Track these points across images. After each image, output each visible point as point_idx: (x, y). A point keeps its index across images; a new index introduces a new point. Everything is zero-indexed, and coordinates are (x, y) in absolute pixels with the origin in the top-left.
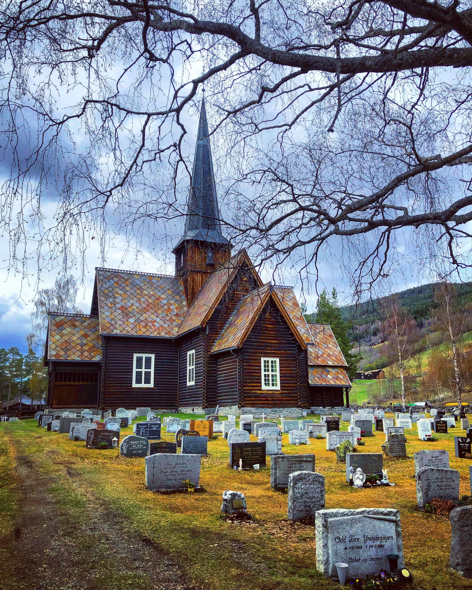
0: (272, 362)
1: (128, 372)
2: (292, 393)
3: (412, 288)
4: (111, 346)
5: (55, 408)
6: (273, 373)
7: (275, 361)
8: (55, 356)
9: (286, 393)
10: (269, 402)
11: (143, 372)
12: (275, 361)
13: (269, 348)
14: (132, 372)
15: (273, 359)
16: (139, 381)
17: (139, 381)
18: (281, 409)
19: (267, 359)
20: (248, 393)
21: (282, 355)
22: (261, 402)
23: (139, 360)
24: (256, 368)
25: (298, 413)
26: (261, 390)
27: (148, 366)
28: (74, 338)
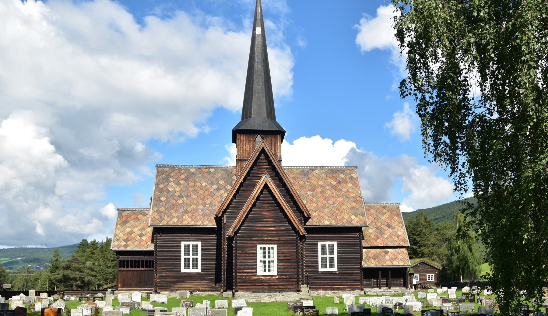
0: (269, 249)
1: (205, 256)
2: (290, 278)
3: (312, 138)
4: (161, 236)
5: (120, 290)
6: (269, 259)
7: (273, 248)
8: (124, 246)
9: (283, 278)
10: (265, 287)
11: (192, 257)
12: (273, 248)
13: (266, 235)
14: (180, 259)
15: (270, 246)
16: (187, 266)
17: (187, 266)
18: (278, 293)
19: (263, 246)
20: (242, 279)
21: (281, 242)
22: (257, 287)
23: (187, 247)
24: (252, 255)
25: (296, 297)
26: (256, 276)
27: (195, 253)
28: (135, 230)
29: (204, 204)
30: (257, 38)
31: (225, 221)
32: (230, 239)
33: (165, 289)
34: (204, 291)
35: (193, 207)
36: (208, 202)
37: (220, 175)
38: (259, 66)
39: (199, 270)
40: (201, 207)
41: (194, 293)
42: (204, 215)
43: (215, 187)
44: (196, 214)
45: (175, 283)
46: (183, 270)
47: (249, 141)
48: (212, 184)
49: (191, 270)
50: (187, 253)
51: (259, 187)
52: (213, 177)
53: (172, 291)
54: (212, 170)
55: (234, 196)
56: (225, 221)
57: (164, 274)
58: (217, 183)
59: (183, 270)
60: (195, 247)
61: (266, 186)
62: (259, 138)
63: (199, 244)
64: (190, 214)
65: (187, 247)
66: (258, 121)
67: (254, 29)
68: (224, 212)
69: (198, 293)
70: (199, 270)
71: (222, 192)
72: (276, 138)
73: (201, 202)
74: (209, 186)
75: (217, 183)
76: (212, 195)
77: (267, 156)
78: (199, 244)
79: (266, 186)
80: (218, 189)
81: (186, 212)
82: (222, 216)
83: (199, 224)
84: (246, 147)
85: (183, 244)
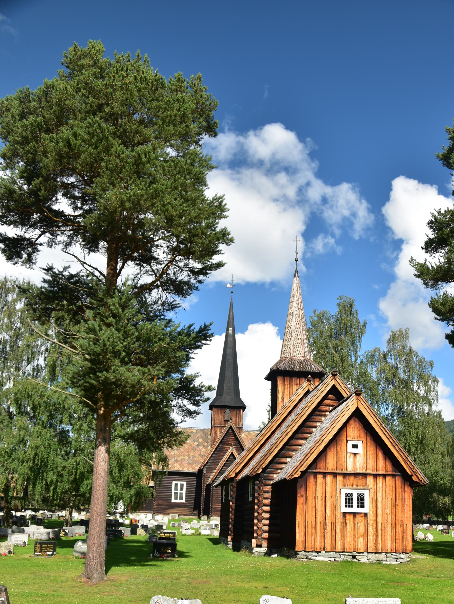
16: (176, 498)
27: (182, 489)
29: (189, 456)
30: (229, 336)
31: (205, 472)
32: (209, 485)
33: (161, 513)
34: (186, 515)
35: (181, 457)
36: (192, 454)
37: (199, 435)
38: (229, 358)
39: (184, 501)
40: (187, 458)
41: (180, 517)
42: (189, 464)
43: (196, 443)
44: (183, 463)
45: (167, 509)
46: (173, 500)
47: (221, 413)
48: (194, 441)
49: (178, 501)
50: (176, 489)
51: (228, 454)
52: (195, 436)
53: (165, 514)
54: (194, 431)
55: (212, 456)
56: (205, 472)
57: (160, 503)
58: (198, 441)
59: (173, 500)
60: (182, 485)
61: (232, 454)
62: (228, 411)
63: (185, 483)
64: (180, 463)
65: (176, 485)
66: (227, 400)
67: (228, 330)
68: (204, 466)
69: (182, 516)
70: (184, 501)
71: (201, 447)
72: (240, 411)
73: (186, 454)
74: (192, 443)
75: (198, 441)
76: (194, 449)
77: (233, 431)
78: (185, 483)
79: (232, 454)
80: (198, 445)
81: (177, 461)
82: (203, 468)
83: (186, 470)
84: (219, 417)
85: (174, 483)
